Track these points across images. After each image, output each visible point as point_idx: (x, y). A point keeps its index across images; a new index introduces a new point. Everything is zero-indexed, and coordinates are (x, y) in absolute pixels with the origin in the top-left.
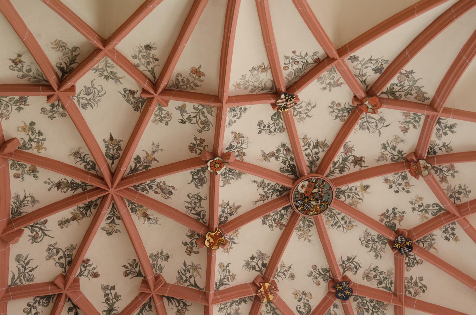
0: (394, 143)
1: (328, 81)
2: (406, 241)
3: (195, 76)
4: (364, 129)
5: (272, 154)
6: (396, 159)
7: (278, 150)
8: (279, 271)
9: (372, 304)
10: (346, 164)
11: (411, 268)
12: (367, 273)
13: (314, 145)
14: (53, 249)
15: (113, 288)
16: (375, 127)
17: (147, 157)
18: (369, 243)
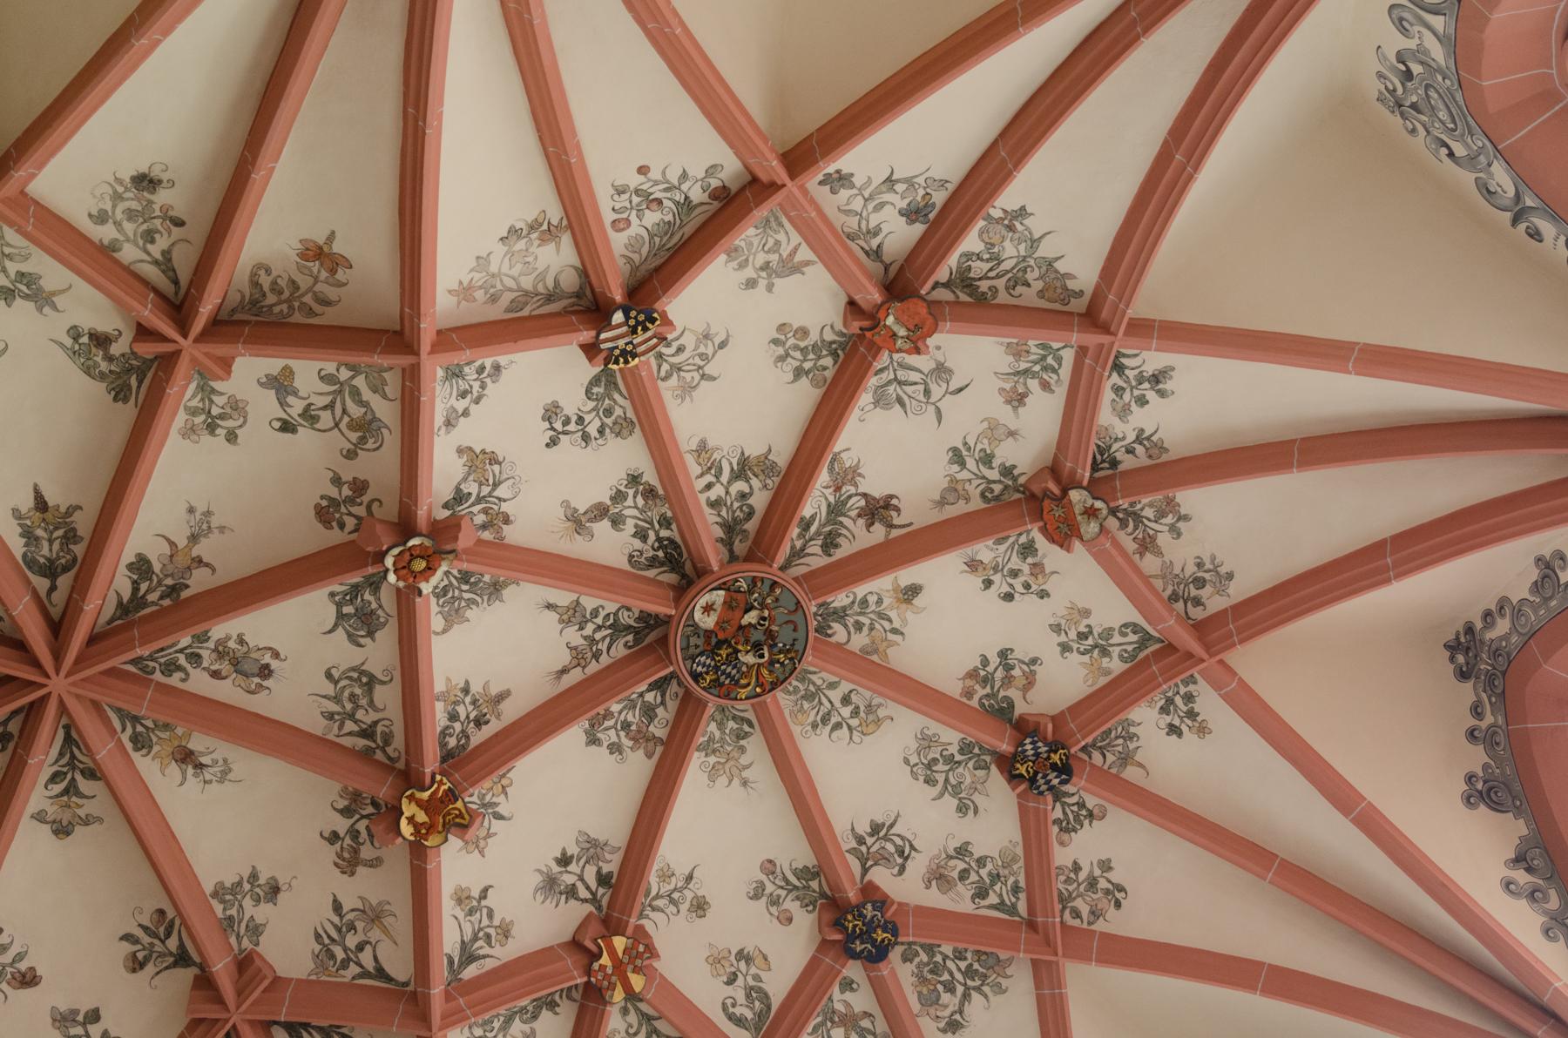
0: (985, 444)
1: (761, 259)
2: (1049, 752)
3: (315, 270)
4: (888, 406)
5: (600, 512)
6: (996, 493)
7: (619, 497)
8: (653, 893)
9: (963, 965)
11: (1073, 834)
13: (732, 469)
16: (921, 397)
17: (172, 556)
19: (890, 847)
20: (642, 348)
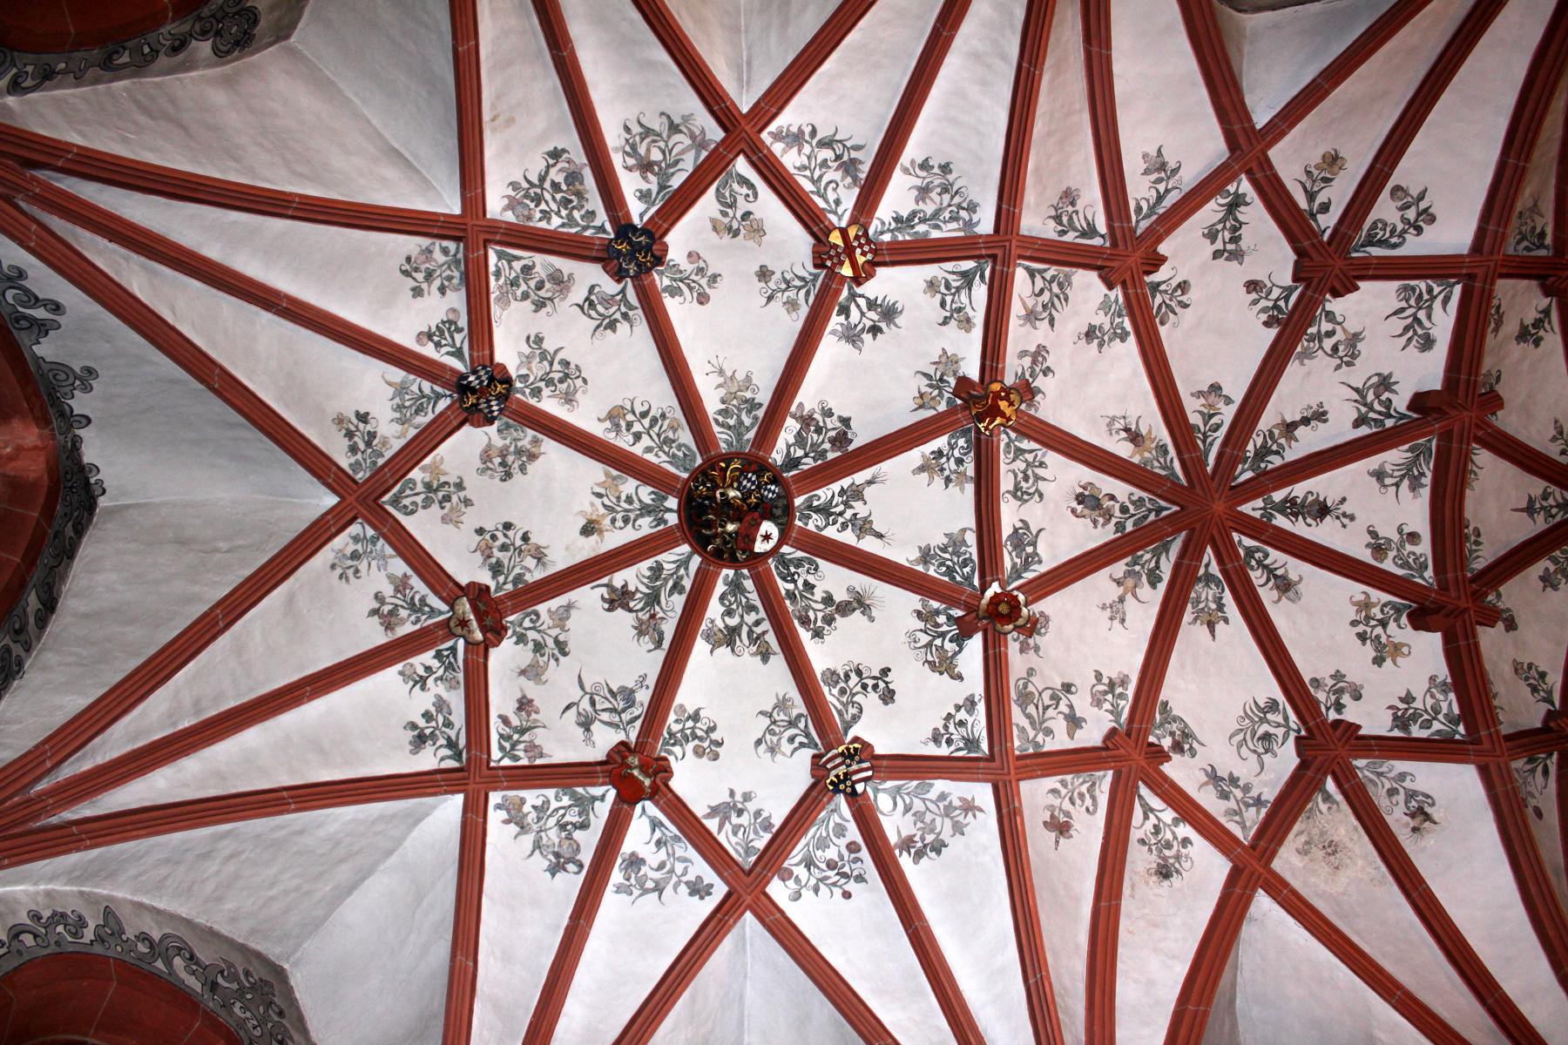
0: (542, 660)
2: (478, 404)
4: (623, 689)
5: (844, 609)
6: (527, 619)
7: (829, 620)
8: (803, 292)
10: (648, 587)
11: (445, 319)
12: (561, 291)
13: (740, 637)
14: (1346, 355)
15: (1217, 255)
17: (1135, 587)
18: (561, 375)
19: (600, 308)
20: (838, 760)
